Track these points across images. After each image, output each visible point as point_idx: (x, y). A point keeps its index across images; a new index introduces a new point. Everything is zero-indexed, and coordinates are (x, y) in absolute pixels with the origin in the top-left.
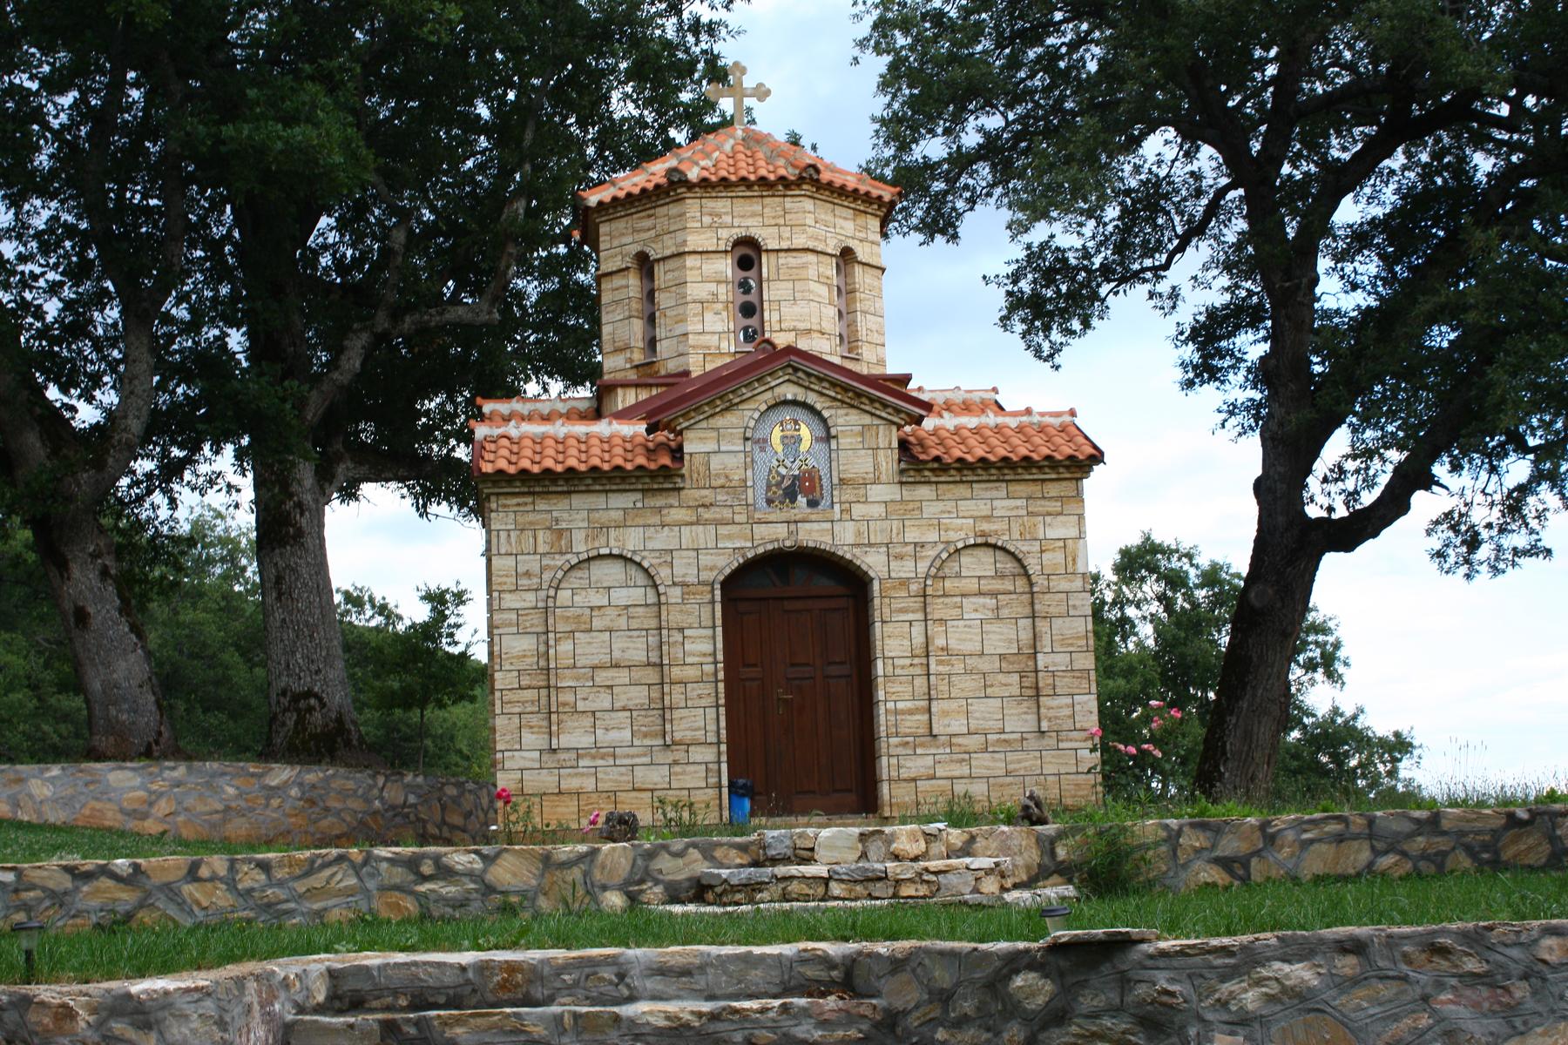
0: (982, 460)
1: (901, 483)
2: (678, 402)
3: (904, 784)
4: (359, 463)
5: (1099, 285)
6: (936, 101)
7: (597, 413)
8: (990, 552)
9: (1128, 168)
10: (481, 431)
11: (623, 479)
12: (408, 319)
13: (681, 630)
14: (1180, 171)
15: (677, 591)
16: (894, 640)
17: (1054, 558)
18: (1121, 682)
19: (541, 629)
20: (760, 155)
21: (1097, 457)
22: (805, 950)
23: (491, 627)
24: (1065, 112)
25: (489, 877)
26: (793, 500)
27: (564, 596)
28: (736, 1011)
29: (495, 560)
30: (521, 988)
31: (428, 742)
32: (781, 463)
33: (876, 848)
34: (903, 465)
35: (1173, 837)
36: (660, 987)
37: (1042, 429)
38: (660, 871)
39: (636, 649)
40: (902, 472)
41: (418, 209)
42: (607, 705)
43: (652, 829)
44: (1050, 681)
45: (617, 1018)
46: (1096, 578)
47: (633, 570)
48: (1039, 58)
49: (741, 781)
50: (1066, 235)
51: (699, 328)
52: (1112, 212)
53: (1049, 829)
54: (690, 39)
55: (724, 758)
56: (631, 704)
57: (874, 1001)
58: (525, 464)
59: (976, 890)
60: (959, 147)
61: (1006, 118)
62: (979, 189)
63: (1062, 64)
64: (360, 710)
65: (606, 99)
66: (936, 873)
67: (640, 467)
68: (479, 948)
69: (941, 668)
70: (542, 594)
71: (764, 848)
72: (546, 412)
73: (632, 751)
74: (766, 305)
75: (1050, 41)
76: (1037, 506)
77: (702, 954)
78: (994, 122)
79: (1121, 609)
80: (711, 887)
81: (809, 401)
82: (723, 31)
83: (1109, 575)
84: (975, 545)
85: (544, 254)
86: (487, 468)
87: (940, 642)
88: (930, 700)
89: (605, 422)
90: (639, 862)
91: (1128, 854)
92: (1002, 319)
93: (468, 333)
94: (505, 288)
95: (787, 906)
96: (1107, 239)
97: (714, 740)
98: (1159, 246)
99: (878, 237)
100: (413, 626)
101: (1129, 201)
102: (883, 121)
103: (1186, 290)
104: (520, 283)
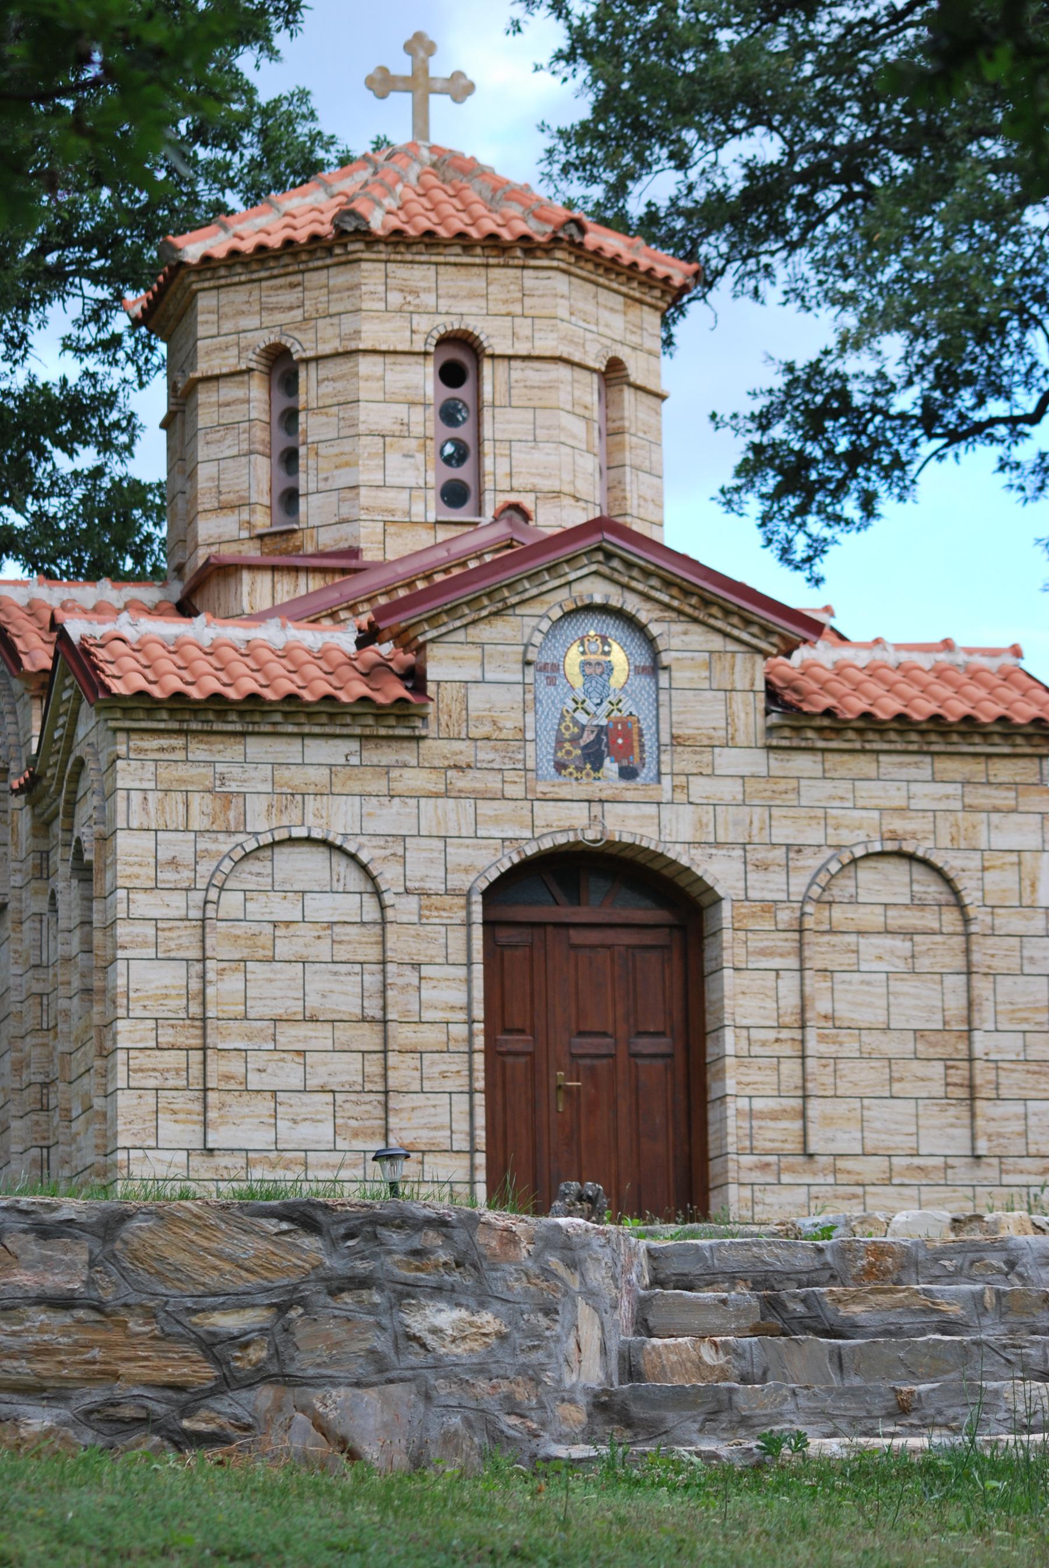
1: (770, 748)
13: (416, 966)
15: (413, 902)
16: (748, 996)
17: (1002, 881)
26: (597, 766)
27: (231, 903)
37: (975, 675)
39: (344, 995)
40: (770, 730)
42: (297, 1083)
44: (991, 1076)
47: (342, 865)
51: (377, 478)
55: (481, 1175)
69: (825, 1049)
70: (198, 897)
73: (335, 1158)
74: (488, 447)
76: (980, 797)
88: (805, 1097)
89: (200, 620)
97: (466, 1146)
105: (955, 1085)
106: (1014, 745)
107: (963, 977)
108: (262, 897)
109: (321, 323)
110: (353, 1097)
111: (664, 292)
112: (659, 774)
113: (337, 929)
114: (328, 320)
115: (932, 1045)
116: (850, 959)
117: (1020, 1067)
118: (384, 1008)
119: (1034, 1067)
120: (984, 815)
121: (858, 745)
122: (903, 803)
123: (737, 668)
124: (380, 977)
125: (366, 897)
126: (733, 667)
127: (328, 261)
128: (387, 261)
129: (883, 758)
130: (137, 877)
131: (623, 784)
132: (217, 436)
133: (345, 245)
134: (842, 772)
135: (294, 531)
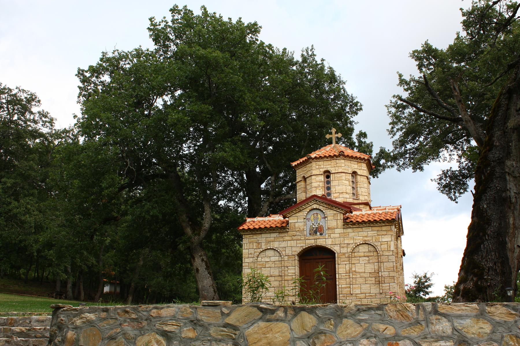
8: (367, 245)
11: (274, 230)
13: (287, 267)
16: (341, 269)
17: (384, 247)
26: (316, 234)
27: (259, 259)
32: (313, 224)
40: (344, 225)
45: (10, 329)
47: (276, 252)
56: (275, 286)
76: (380, 233)
84: (363, 244)
87: (353, 269)
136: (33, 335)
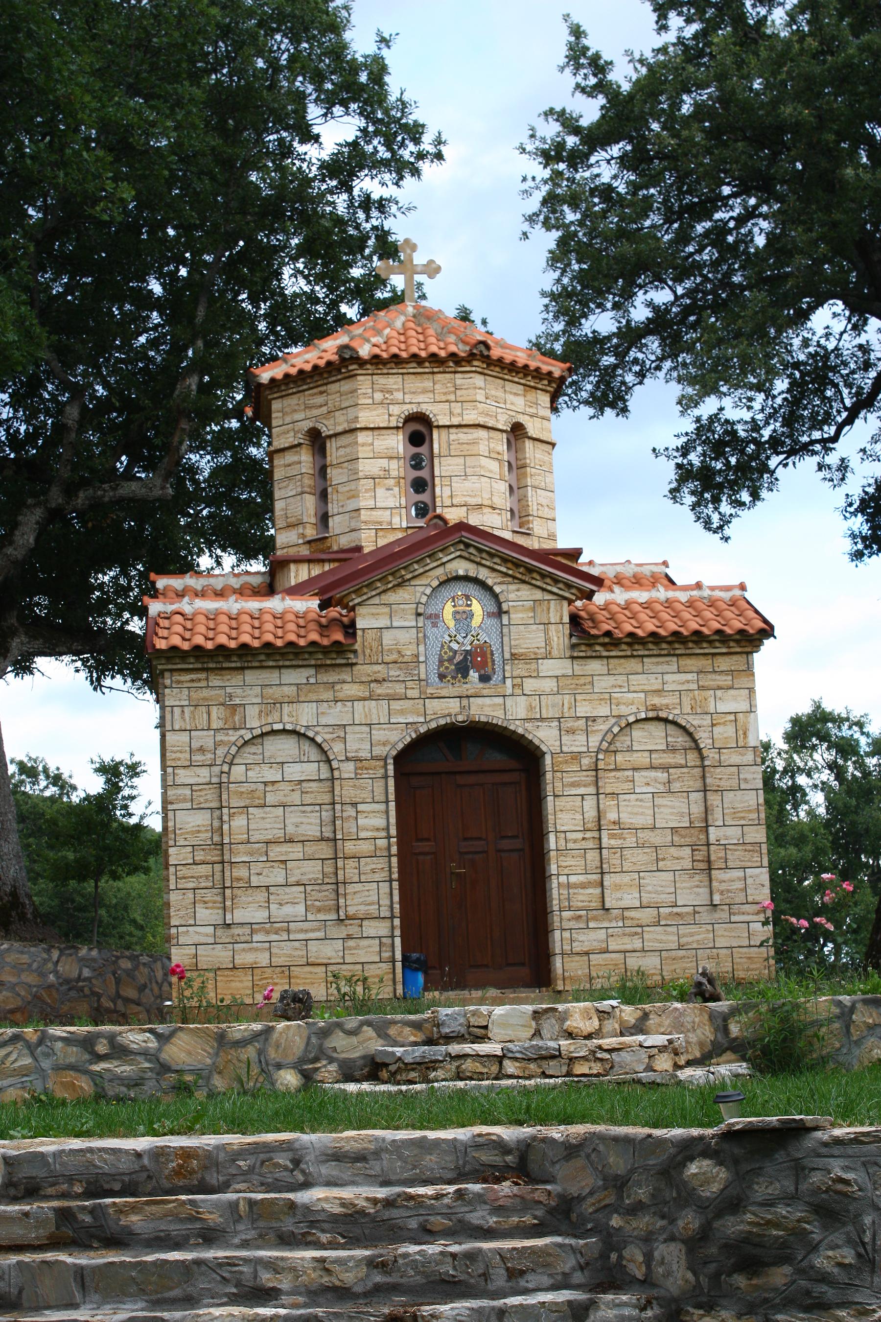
0: (653, 634)
2: (351, 577)
3: (577, 958)
4: (33, 637)
5: (768, 458)
6: (605, 276)
7: (270, 589)
8: (661, 726)
9: (797, 342)
10: (155, 607)
12: (81, 494)
13: (354, 805)
14: (849, 343)
15: (350, 766)
16: (566, 814)
18: (793, 850)
19: (215, 804)
20: (431, 332)
21: (767, 631)
22: (480, 1135)
23: (165, 802)
24: (733, 285)
25: (164, 1056)
26: (465, 675)
27: (238, 772)
28: (411, 1197)
29: (169, 736)
30: (197, 1174)
31: (102, 912)
33: (549, 1026)
34: (574, 640)
35: (846, 1014)
36: (334, 1173)
37: (712, 603)
38: (334, 1049)
39: (309, 825)
40: (573, 647)
41: (91, 385)
42: (281, 880)
43: (328, 1005)
46: (767, 747)
47: (306, 746)
48: (707, 233)
49: (415, 956)
50: (733, 408)
51: (371, 503)
52: (781, 385)
53: (722, 1006)
54: (361, 215)
55: (397, 932)
56: (304, 879)
57: (549, 1187)
58: (199, 640)
59: (650, 1068)
60: (628, 322)
61: (675, 292)
62: (648, 363)
63: (730, 239)
64: (34, 880)
65: (278, 275)
66: (609, 1051)
67: (313, 643)
68: (156, 1134)
69: (613, 842)
70: (216, 769)
71: (438, 1026)
72: (219, 587)
75: (718, 216)
76: (709, 680)
77: (376, 1139)
78: (663, 296)
79: (792, 777)
80: (386, 1065)
81: (480, 577)
82: (394, 208)
83: (779, 744)
84: (646, 719)
85: (216, 428)
86: (161, 644)
87: (612, 816)
88: (602, 873)
89: (278, 597)
90: (314, 1040)
91: (801, 1031)
92: (671, 491)
93: (141, 508)
94: (178, 463)
95: (461, 1084)
96: (776, 411)
97: (388, 914)
98: (828, 419)
99: (547, 413)
100: (88, 798)
101: (797, 374)
102: (553, 296)
103: (854, 462)
104: (194, 457)
105: (699, 861)
106: (729, 647)
107: (702, 793)
108: (257, 768)
109: (337, 413)
110: (317, 887)
111: (550, 382)
112: (504, 678)
113: (304, 785)
114: (341, 412)
115: (683, 836)
116: (628, 786)
117: (740, 848)
118: (335, 832)
119: (749, 847)
120: (712, 692)
121: (629, 653)
122: (660, 688)
123: (552, 610)
124: (331, 813)
125: (321, 764)
126: (549, 609)
127: (339, 377)
128: (373, 374)
129: (645, 660)
130: (179, 759)
131: (481, 685)
132: (284, 484)
133: (347, 367)
134: (620, 670)
135: (326, 538)
136: (413, 1224)
